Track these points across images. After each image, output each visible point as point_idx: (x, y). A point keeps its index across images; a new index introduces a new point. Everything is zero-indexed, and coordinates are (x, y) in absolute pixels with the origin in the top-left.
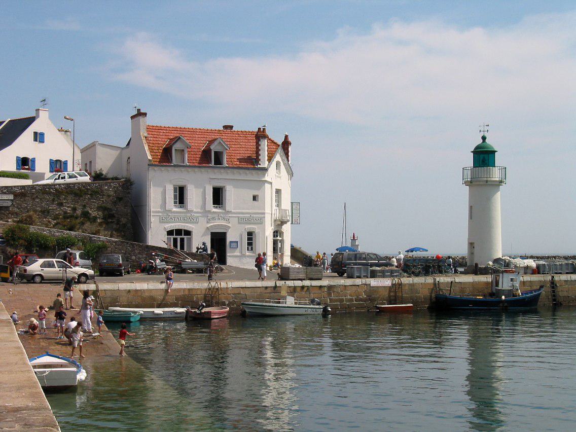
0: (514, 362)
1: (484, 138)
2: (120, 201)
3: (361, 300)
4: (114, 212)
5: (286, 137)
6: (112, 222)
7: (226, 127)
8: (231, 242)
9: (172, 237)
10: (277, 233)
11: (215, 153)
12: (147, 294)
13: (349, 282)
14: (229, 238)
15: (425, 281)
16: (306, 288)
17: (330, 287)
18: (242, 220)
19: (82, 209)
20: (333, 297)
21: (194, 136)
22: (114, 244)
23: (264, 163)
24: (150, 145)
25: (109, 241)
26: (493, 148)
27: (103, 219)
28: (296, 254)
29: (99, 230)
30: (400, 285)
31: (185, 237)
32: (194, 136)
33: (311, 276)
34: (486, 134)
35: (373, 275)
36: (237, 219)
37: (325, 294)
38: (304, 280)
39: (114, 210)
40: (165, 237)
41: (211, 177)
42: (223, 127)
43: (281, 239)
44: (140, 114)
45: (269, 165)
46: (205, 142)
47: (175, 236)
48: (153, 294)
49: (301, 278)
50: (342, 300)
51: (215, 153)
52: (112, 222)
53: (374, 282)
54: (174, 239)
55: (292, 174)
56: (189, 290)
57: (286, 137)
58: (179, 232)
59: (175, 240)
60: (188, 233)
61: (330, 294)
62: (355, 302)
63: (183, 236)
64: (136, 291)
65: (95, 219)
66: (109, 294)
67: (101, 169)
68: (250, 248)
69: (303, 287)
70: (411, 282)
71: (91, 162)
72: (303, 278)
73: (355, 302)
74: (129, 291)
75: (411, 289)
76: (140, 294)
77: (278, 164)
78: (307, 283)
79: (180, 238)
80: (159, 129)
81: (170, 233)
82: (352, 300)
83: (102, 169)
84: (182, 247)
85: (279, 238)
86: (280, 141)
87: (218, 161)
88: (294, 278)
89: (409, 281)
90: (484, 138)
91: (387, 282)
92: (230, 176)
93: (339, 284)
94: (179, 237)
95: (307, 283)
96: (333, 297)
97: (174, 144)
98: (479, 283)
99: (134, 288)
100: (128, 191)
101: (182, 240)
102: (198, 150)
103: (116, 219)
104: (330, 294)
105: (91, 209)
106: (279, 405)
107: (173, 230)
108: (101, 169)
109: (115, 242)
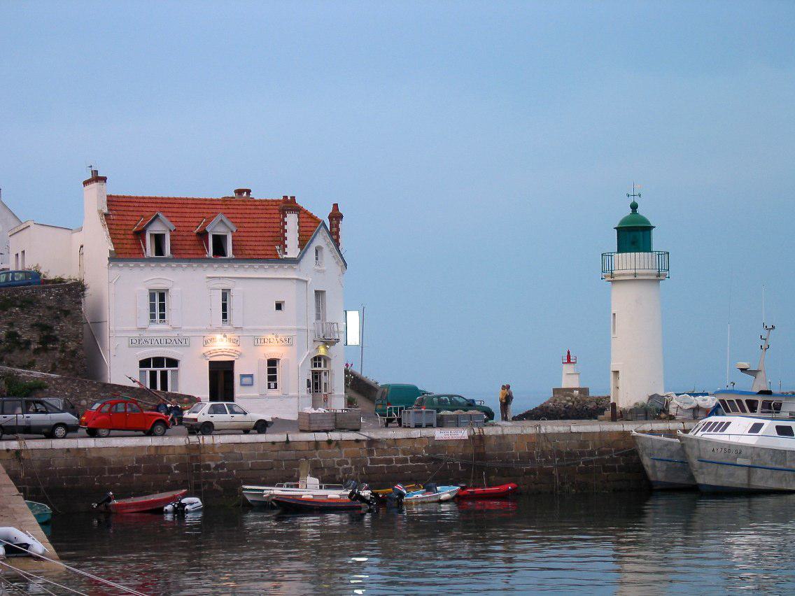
0: (489, 590)
1: (634, 207)
2: (66, 316)
3: (419, 460)
4: (57, 332)
5: (336, 206)
6: (54, 349)
7: (239, 192)
8: (243, 376)
9: (148, 370)
10: (320, 359)
11: (215, 237)
12: (94, 454)
13: (400, 434)
14: (238, 371)
15: (522, 431)
16: (333, 444)
17: (372, 442)
18: (259, 342)
19: (8, 329)
20: (375, 456)
21: (183, 210)
22: (54, 382)
23: (292, 250)
24: (113, 227)
25: (48, 379)
26: (648, 222)
27: (40, 343)
28: (357, 385)
29: (34, 360)
30: (481, 438)
31: (169, 370)
32: (183, 210)
33: (340, 426)
34: (637, 200)
35: (441, 423)
36: (252, 338)
37: (363, 453)
38: (331, 431)
39: (57, 330)
40: (135, 372)
41: (144, 280)
42: (236, 191)
43: (326, 369)
44: (97, 178)
45: (302, 256)
46: (200, 220)
47: (152, 369)
48: (103, 454)
49: (327, 428)
50: (390, 461)
51: (215, 237)
52: (54, 349)
53: (440, 434)
54: (151, 372)
55: (346, 265)
56: (157, 447)
57: (336, 206)
58: (158, 361)
59: (153, 374)
60: (173, 363)
61: (370, 452)
62: (410, 464)
63: (165, 369)
64: (79, 450)
65: (28, 343)
66: (38, 455)
67: (38, 265)
68: (272, 385)
69: (330, 442)
70: (500, 433)
71: (23, 252)
72: (332, 428)
73: (410, 464)
74: (68, 450)
75: (500, 444)
76: (83, 455)
77: (318, 250)
78: (335, 436)
79: (162, 372)
80: (128, 201)
81: (144, 363)
82: (405, 460)
83: (40, 265)
84: (164, 386)
85: (322, 368)
86: (323, 214)
87: (219, 249)
88: (316, 429)
89: (497, 432)
90: (634, 207)
91: (463, 434)
92: (241, 273)
93: (385, 437)
94: (159, 370)
95: (335, 436)
96: (375, 456)
97: (147, 226)
98: (610, 433)
99: (75, 447)
100: (78, 300)
101: (164, 374)
102: (190, 233)
103: (60, 343)
104: (370, 452)
105: (21, 328)
106: (410, 564)
107: (149, 359)
108: (38, 265)
109: (56, 379)
